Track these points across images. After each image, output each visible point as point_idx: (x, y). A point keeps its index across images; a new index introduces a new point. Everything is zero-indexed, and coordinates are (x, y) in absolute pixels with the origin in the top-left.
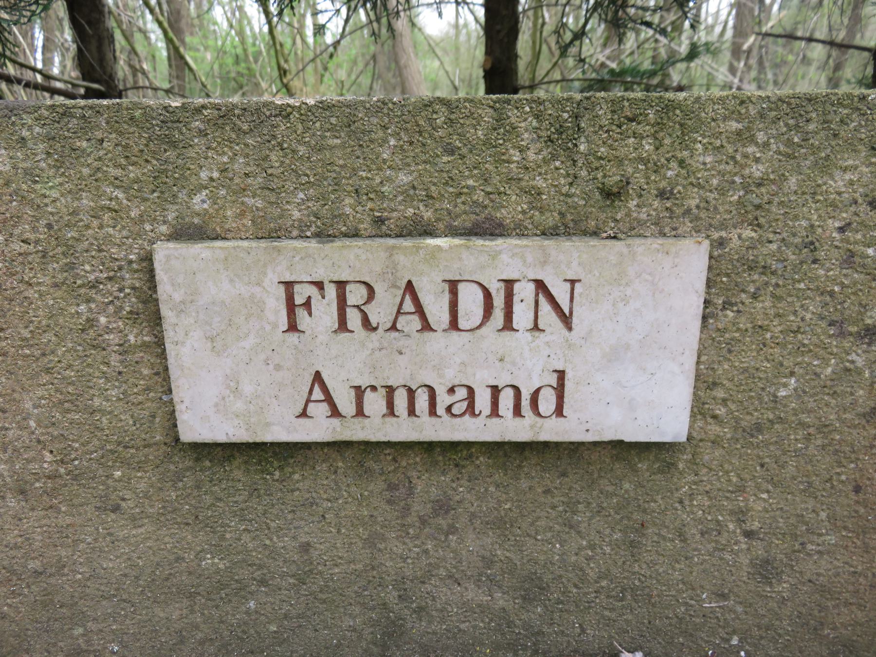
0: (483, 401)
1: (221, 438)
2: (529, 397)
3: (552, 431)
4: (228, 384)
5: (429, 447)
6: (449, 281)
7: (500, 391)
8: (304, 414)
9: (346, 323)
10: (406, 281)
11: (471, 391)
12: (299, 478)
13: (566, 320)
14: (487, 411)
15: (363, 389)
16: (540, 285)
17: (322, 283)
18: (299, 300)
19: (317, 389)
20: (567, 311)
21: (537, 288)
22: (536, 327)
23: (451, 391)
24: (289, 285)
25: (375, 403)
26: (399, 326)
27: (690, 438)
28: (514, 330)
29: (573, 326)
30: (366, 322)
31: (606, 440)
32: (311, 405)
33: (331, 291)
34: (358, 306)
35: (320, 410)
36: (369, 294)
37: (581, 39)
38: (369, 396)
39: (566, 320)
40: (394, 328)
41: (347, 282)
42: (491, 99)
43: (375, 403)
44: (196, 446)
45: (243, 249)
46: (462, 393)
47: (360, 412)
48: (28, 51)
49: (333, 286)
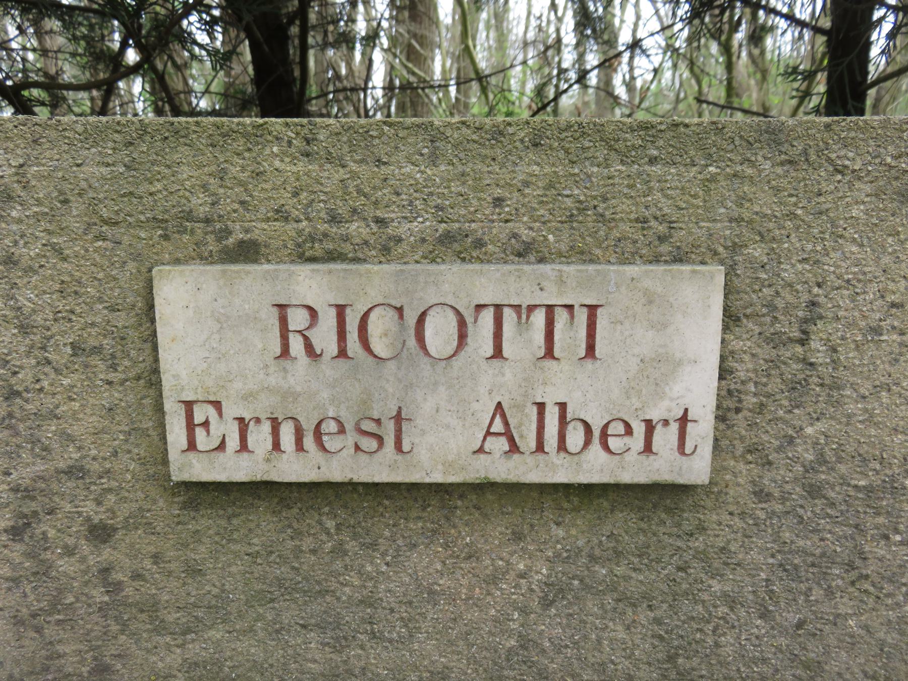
1: (293, 478)
2: (599, 430)
3: (380, 469)
5: (351, 487)
7: (567, 424)
8: (481, 450)
15: (654, 423)
17: (219, 402)
18: (198, 418)
19: (498, 419)
25: (260, 437)
27: (710, 483)
30: (309, 348)
31: (287, 480)
32: (488, 439)
33: (582, 316)
34: (299, 332)
35: (500, 445)
38: (659, 430)
43: (260, 437)
44: (188, 485)
45: (235, 272)
48: (846, 80)
49: (585, 310)
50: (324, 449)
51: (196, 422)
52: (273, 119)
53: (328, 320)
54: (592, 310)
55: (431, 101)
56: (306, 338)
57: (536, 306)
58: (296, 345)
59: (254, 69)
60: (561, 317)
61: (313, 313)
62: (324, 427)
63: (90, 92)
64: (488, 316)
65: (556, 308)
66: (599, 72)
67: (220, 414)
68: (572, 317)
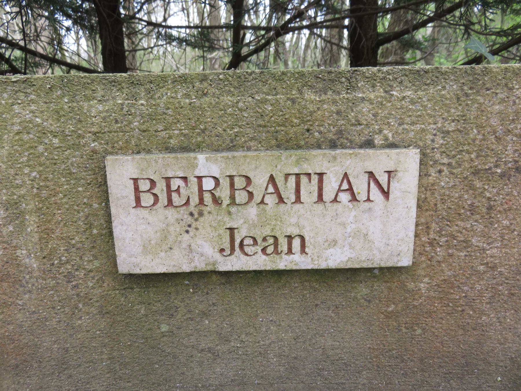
0: (284, 246)
4: (142, 240)
5: (258, 274)
6: (368, 172)
9: (300, 198)
10: (269, 175)
11: (276, 238)
12: (363, 290)
13: (386, 194)
14: (285, 248)
15: (293, 236)
16: (371, 174)
18: (174, 187)
20: (386, 190)
21: (369, 177)
22: (368, 200)
23: (264, 239)
24: (135, 180)
26: (338, 200)
28: (337, 201)
29: (390, 199)
30: (216, 201)
33: (315, 179)
36: (216, 184)
37: (506, 30)
39: (386, 194)
40: (335, 200)
41: (391, 171)
42: (399, 69)
44: (134, 279)
46: (271, 241)
47: (290, 251)
50: (247, 254)
51: (204, 189)
52: (111, 74)
53: (225, 183)
54: (321, 175)
55: (290, 46)
56: (213, 195)
57: (289, 174)
58: (207, 198)
59: (123, 42)
60: (304, 180)
61: (153, 183)
62: (246, 242)
63: (231, 47)
64: (292, 180)
65: (301, 176)
66: (392, 15)
67: (187, 185)
68: (310, 180)
